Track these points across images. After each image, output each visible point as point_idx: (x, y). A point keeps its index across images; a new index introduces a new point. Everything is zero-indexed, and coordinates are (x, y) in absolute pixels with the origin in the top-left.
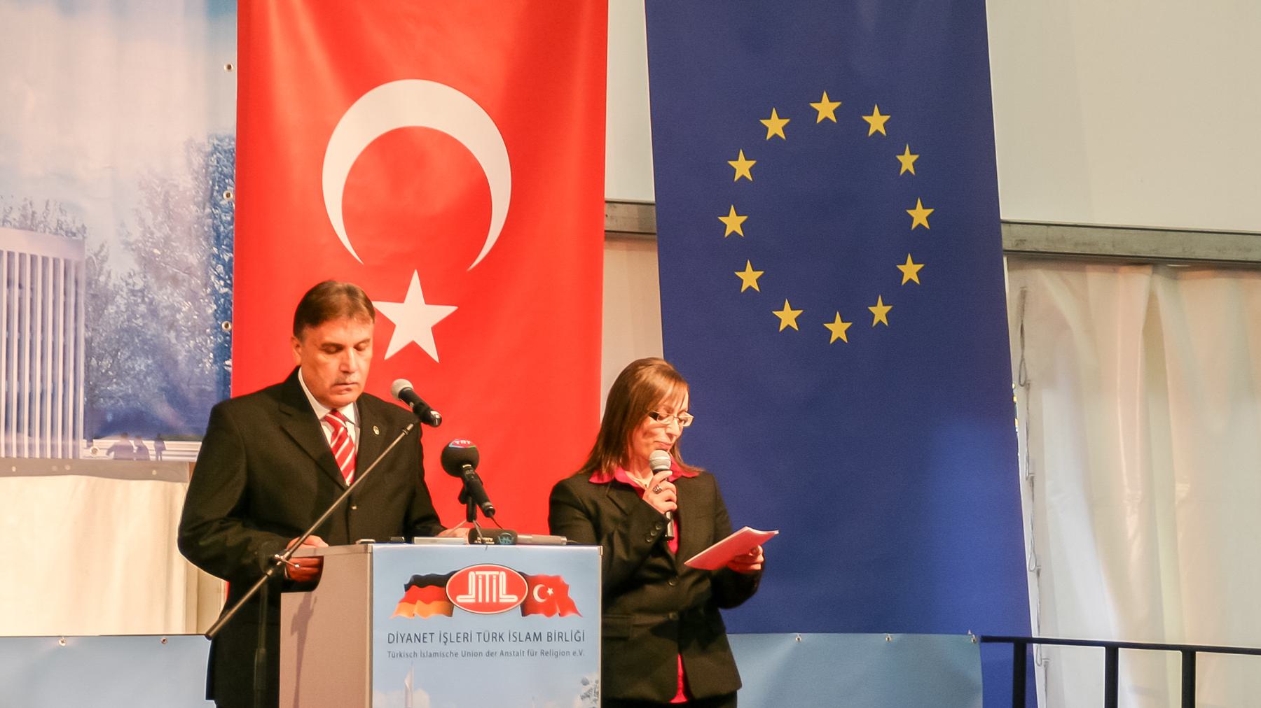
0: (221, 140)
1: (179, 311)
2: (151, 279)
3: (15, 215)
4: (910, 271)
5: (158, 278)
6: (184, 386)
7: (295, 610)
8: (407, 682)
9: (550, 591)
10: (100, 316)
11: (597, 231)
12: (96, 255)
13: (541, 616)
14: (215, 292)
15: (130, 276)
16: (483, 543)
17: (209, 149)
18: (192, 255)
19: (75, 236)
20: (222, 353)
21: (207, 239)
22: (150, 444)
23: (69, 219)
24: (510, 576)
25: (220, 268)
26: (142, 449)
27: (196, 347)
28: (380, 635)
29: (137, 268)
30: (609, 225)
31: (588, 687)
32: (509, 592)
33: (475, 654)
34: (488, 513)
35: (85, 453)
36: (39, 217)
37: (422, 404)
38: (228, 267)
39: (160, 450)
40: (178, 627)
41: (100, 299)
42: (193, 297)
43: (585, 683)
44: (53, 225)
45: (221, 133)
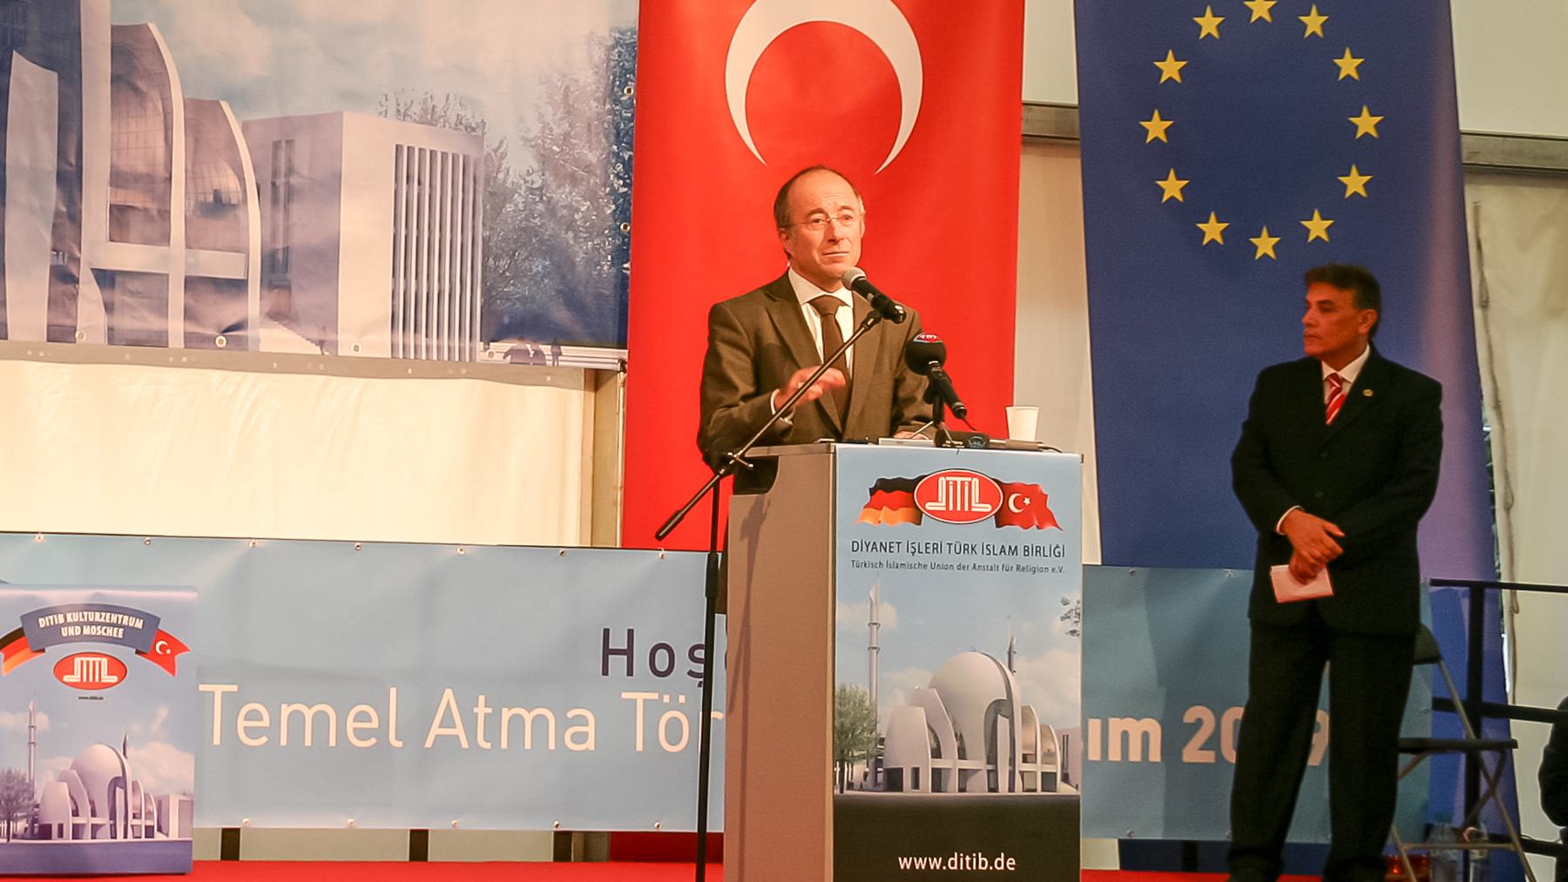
0: (622, 33)
1: (577, 210)
2: (549, 178)
3: (416, 109)
4: (1355, 183)
5: (556, 176)
6: (581, 288)
7: (746, 514)
8: (872, 595)
9: (1027, 501)
10: (499, 214)
11: (1018, 132)
12: (496, 151)
13: (1017, 528)
14: (614, 191)
15: (528, 174)
16: (953, 446)
17: (611, 42)
18: (593, 154)
19: (474, 132)
20: (621, 255)
21: (607, 137)
22: (546, 349)
23: (469, 115)
24: (984, 482)
25: (620, 167)
26: (538, 353)
27: (594, 248)
28: (843, 543)
29: (536, 166)
30: (1026, 129)
31: (1068, 608)
32: (110, 673)
33: (946, 567)
34: (959, 414)
35: (482, 356)
36: (439, 110)
37: (883, 297)
38: (627, 165)
39: (557, 355)
40: (572, 539)
41: (499, 197)
42: (592, 197)
43: (1065, 603)
44: (453, 120)
45: (623, 26)
